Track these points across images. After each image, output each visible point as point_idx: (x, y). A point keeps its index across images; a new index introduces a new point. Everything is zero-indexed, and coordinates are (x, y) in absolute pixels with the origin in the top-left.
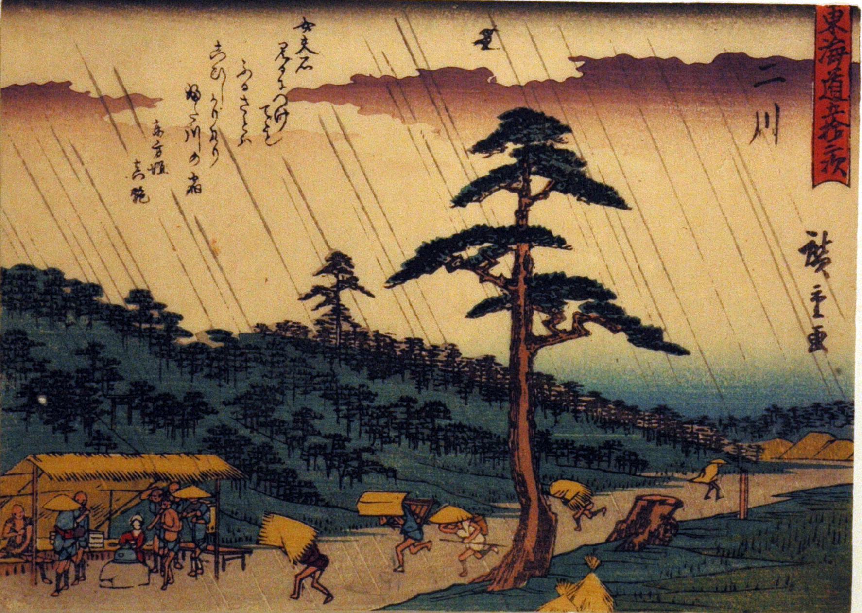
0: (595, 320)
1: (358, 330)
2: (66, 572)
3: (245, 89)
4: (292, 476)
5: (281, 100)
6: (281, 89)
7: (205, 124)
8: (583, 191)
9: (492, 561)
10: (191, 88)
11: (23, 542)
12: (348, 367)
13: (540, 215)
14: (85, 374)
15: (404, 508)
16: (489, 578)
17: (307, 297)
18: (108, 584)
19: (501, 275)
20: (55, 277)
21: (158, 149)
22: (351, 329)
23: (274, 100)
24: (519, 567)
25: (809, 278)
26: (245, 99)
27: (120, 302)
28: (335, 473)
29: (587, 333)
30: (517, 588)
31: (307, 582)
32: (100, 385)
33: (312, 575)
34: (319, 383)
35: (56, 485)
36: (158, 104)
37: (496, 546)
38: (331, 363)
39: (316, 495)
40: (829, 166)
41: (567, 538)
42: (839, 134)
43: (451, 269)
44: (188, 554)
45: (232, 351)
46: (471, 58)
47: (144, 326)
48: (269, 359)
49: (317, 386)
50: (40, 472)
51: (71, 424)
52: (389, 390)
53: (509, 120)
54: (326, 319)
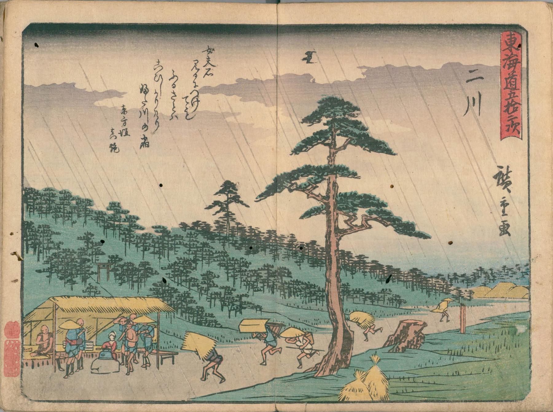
0: (375, 219)
3: (174, 87)
4: (201, 311)
5: (195, 94)
6: (195, 87)
7: (151, 106)
8: (366, 145)
9: (317, 359)
10: (143, 86)
15: (266, 328)
16: (316, 368)
17: (210, 207)
18: (96, 371)
19: (320, 194)
20: (66, 196)
21: (125, 121)
22: (236, 226)
23: (191, 93)
24: (332, 362)
25: (499, 193)
26: (174, 93)
27: (104, 210)
28: (226, 309)
29: (370, 227)
30: (332, 375)
31: (210, 371)
32: (91, 256)
33: (213, 367)
34: (216, 257)
35: (65, 315)
36: (124, 95)
37: (318, 351)
38: (224, 245)
39: (216, 322)
40: (510, 128)
41: (359, 346)
42: (515, 110)
43: (291, 191)
44: (141, 355)
45: (166, 238)
47: (116, 223)
48: (188, 243)
49: (216, 259)
50: (57, 307)
51: (74, 280)
52: (258, 261)
54: (221, 220)
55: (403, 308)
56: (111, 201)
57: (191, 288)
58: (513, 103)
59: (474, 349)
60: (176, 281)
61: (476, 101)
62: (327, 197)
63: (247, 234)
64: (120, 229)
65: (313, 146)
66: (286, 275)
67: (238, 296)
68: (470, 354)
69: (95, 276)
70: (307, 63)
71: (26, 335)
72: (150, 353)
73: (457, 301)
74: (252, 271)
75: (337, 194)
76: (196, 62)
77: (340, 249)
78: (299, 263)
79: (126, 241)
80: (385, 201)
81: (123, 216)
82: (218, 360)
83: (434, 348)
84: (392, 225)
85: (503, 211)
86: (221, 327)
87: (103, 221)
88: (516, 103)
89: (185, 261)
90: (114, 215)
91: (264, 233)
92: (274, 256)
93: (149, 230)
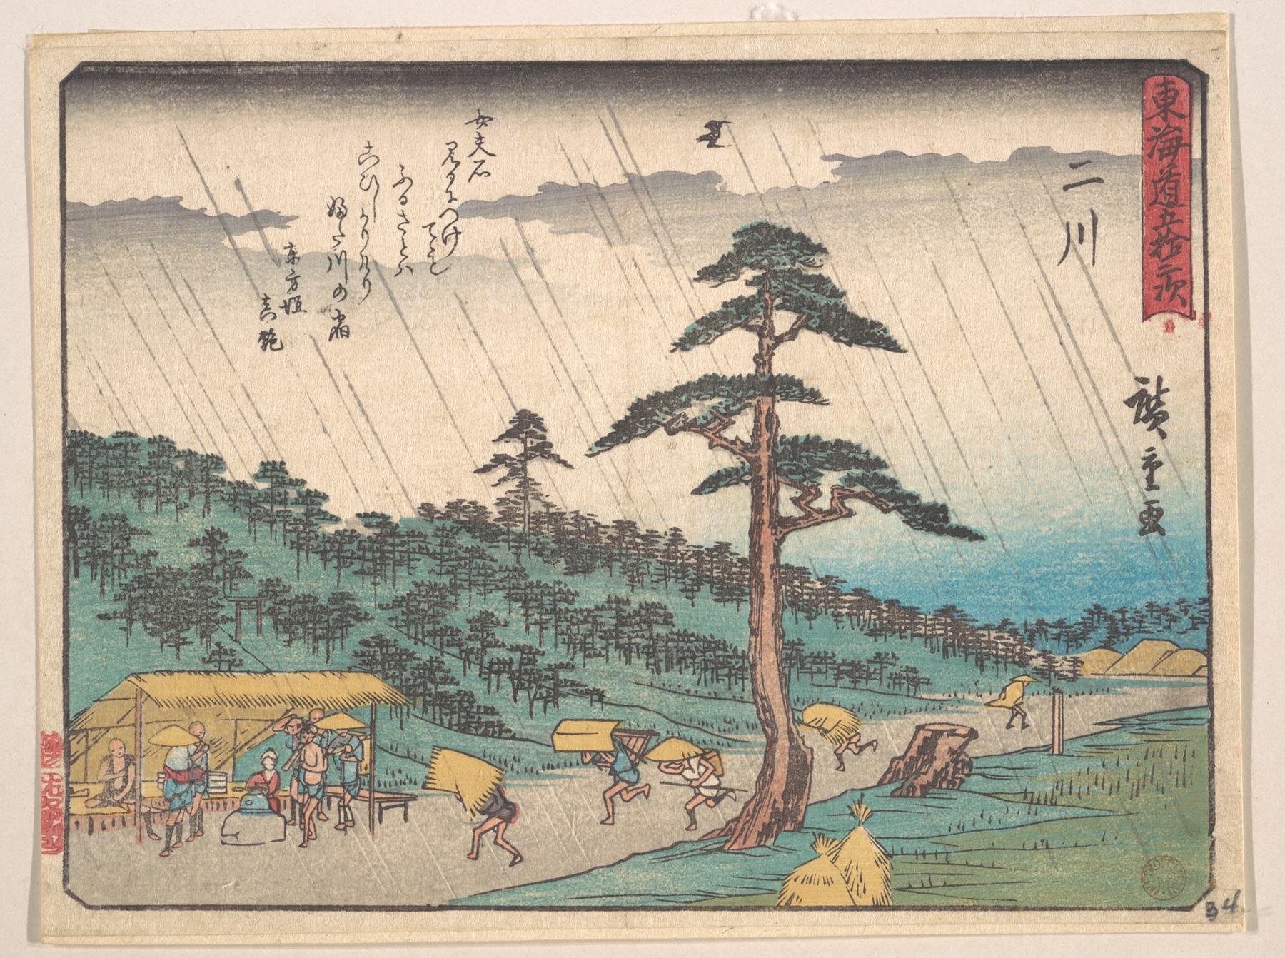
0: (861, 496)
3: (403, 203)
9: (729, 809)
17: (486, 469)
18: (234, 840)
20: (163, 446)
21: (294, 281)
22: (544, 510)
24: (764, 817)
25: (1141, 438)
29: (850, 514)
33: (495, 828)
38: (518, 555)
40: (1164, 292)
42: (1176, 251)
44: (335, 801)
49: (500, 585)
52: (593, 590)
54: (512, 497)
55: (925, 696)
57: (446, 649)
58: (1171, 236)
59: (1084, 789)
60: (412, 632)
61: (1080, 235)
62: (755, 446)
63: (570, 528)
64: (285, 522)
65: (722, 332)
66: (661, 620)
67: (549, 667)
68: (1074, 799)
69: (230, 627)
70: (709, 146)
71: (74, 761)
72: (353, 797)
73: (1045, 682)
74: (581, 611)
75: (775, 440)
76: (452, 146)
77: (783, 562)
78: (690, 593)
79: (299, 548)
80: (883, 457)
81: (293, 494)
82: (506, 812)
83: (992, 786)
84: (899, 509)
85: (1150, 479)
86: (513, 738)
87: (250, 504)
88: (1178, 237)
89: (433, 587)
90: (271, 489)
91: (607, 527)
92: (632, 578)
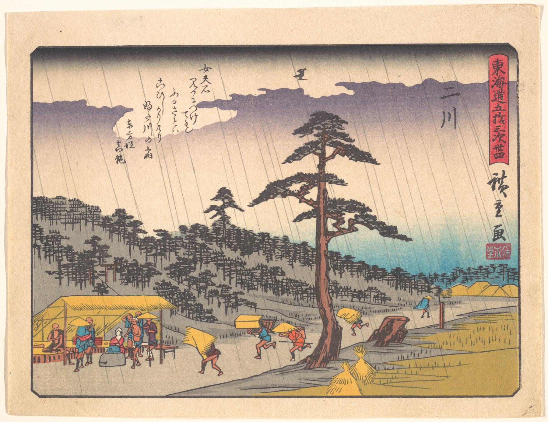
1: (235, 228)
2: (82, 359)
9: (308, 352)
11: (59, 342)
12: (230, 249)
13: (330, 168)
14: (92, 253)
17: (207, 212)
25: (494, 196)
29: (357, 230)
43: (284, 196)
44: (145, 349)
46: (293, 84)
52: (255, 260)
53: (314, 117)
56: (117, 208)
65: (305, 155)
93: (151, 234)
